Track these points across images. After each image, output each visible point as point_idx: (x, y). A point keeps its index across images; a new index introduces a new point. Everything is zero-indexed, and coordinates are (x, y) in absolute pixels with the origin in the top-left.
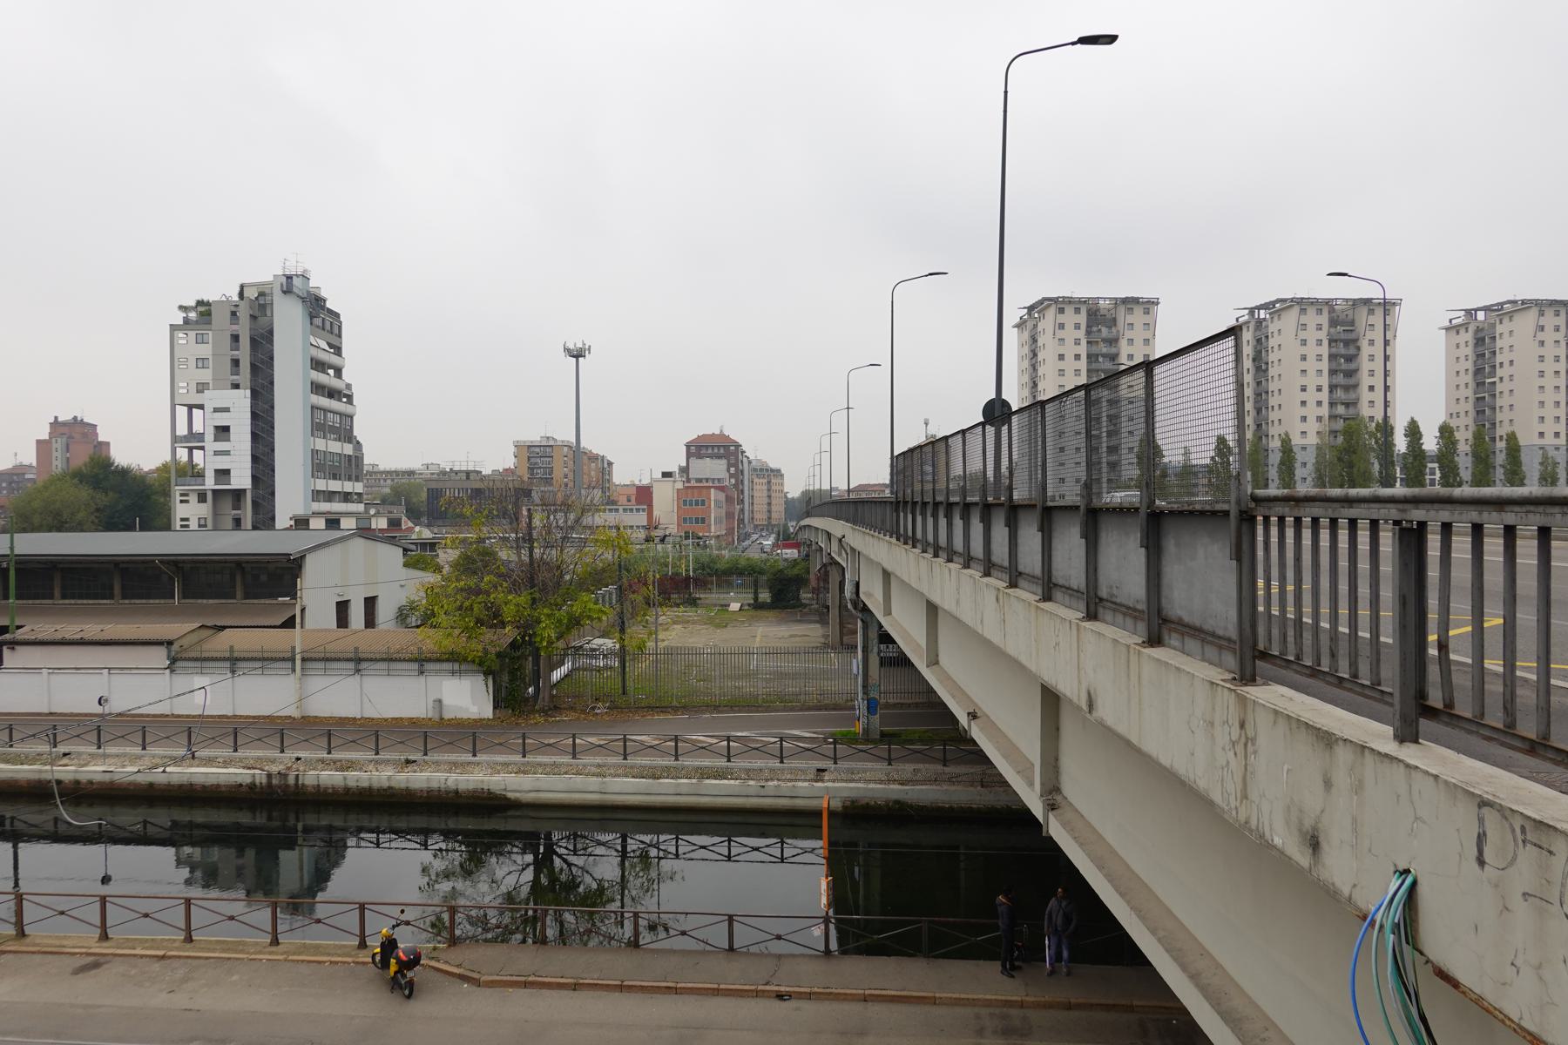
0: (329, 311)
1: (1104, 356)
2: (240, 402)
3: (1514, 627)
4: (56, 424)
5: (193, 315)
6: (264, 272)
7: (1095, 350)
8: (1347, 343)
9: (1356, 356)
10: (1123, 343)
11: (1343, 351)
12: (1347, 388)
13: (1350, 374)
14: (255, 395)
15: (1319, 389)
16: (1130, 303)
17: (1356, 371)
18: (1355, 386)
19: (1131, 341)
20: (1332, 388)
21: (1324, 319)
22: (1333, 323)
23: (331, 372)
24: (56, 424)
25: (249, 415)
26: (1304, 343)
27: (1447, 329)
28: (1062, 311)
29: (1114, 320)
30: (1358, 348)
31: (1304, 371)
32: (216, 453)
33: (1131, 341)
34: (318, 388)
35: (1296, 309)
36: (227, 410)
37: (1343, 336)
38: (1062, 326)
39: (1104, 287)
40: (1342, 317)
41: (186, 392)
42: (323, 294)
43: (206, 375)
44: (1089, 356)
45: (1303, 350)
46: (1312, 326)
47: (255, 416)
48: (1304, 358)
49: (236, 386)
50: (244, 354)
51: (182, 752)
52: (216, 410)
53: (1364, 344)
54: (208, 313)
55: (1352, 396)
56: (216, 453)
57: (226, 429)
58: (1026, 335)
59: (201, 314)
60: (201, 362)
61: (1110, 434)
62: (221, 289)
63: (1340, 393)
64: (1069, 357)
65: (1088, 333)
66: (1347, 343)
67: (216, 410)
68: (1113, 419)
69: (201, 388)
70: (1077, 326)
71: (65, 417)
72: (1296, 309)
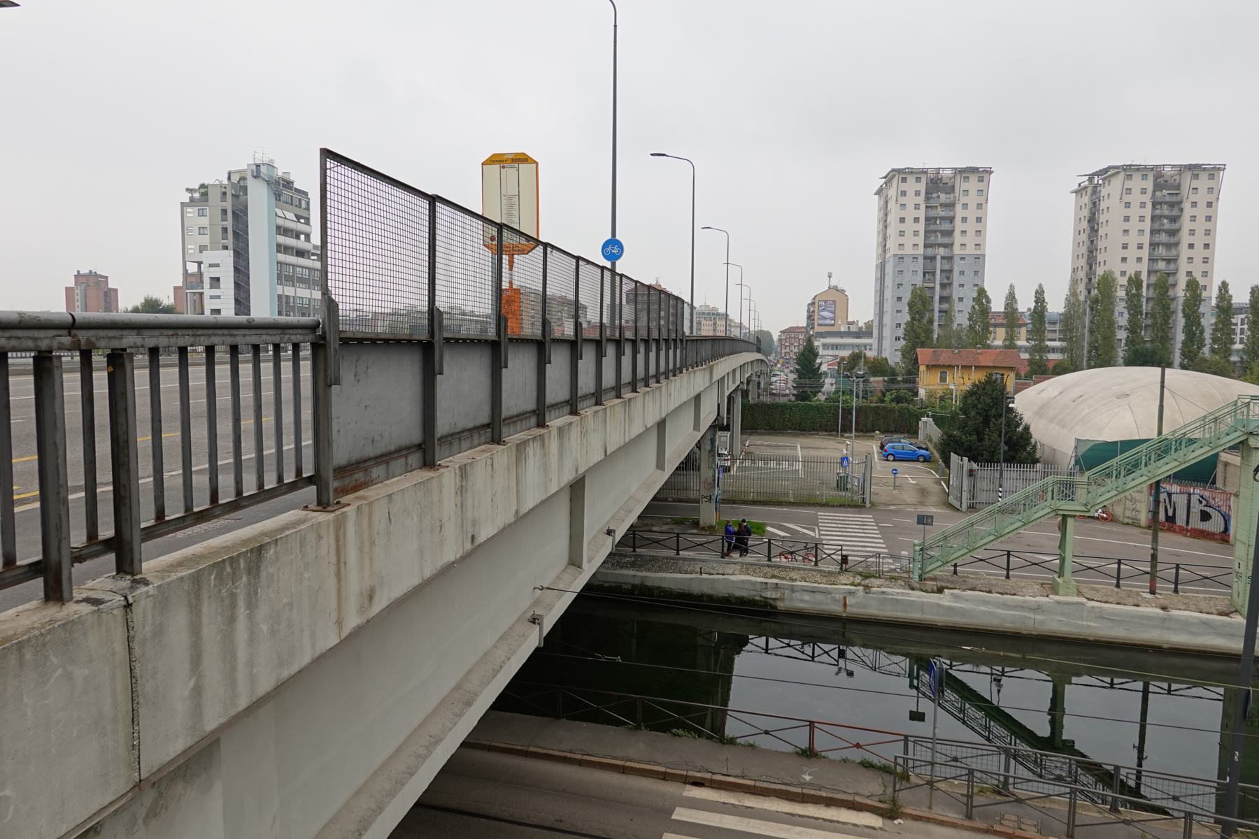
0: (298, 191)
1: (942, 218)
2: (227, 258)
3: (210, 456)
4: (78, 276)
5: (197, 195)
6: (242, 163)
7: (932, 213)
8: (1172, 205)
9: (1179, 217)
10: (958, 207)
11: (1166, 212)
12: (1169, 246)
13: (1173, 233)
14: (237, 254)
15: (1140, 247)
16: (1195, 169)
17: (1178, 230)
18: (1177, 244)
19: (965, 206)
20: (1154, 245)
21: (1149, 184)
22: (1158, 187)
23: (302, 237)
24: (78, 276)
25: (232, 269)
26: (1128, 205)
27: (1076, 192)
28: (904, 180)
29: (953, 187)
30: (1182, 210)
31: (1126, 231)
32: (211, 297)
33: (965, 206)
34: (281, 248)
35: (1122, 175)
36: (218, 265)
37: (1168, 199)
38: (904, 193)
39: (1169, 156)
40: (1171, 181)
41: (192, 248)
42: (292, 178)
43: (205, 240)
44: (927, 219)
45: (1127, 212)
46: (910, 193)
47: (237, 270)
48: (1127, 219)
49: (226, 248)
50: (229, 223)
51: (1149, 569)
52: (211, 266)
53: (1187, 206)
54: (205, 194)
55: (1173, 252)
56: (211, 297)
57: (218, 279)
58: (1086, 199)
59: (203, 194)
60: (201, 230)
61: (943, 286)
62: (216, 175)
63: (1162, 251)
64: (909, 220)
65: (927, 199)
66: (1172, 205)
67: (211, 266)
68: (948, 273)
69: (202, 249)
70: (917, 193)
71: (84, 271)
72: (1122, 175)
